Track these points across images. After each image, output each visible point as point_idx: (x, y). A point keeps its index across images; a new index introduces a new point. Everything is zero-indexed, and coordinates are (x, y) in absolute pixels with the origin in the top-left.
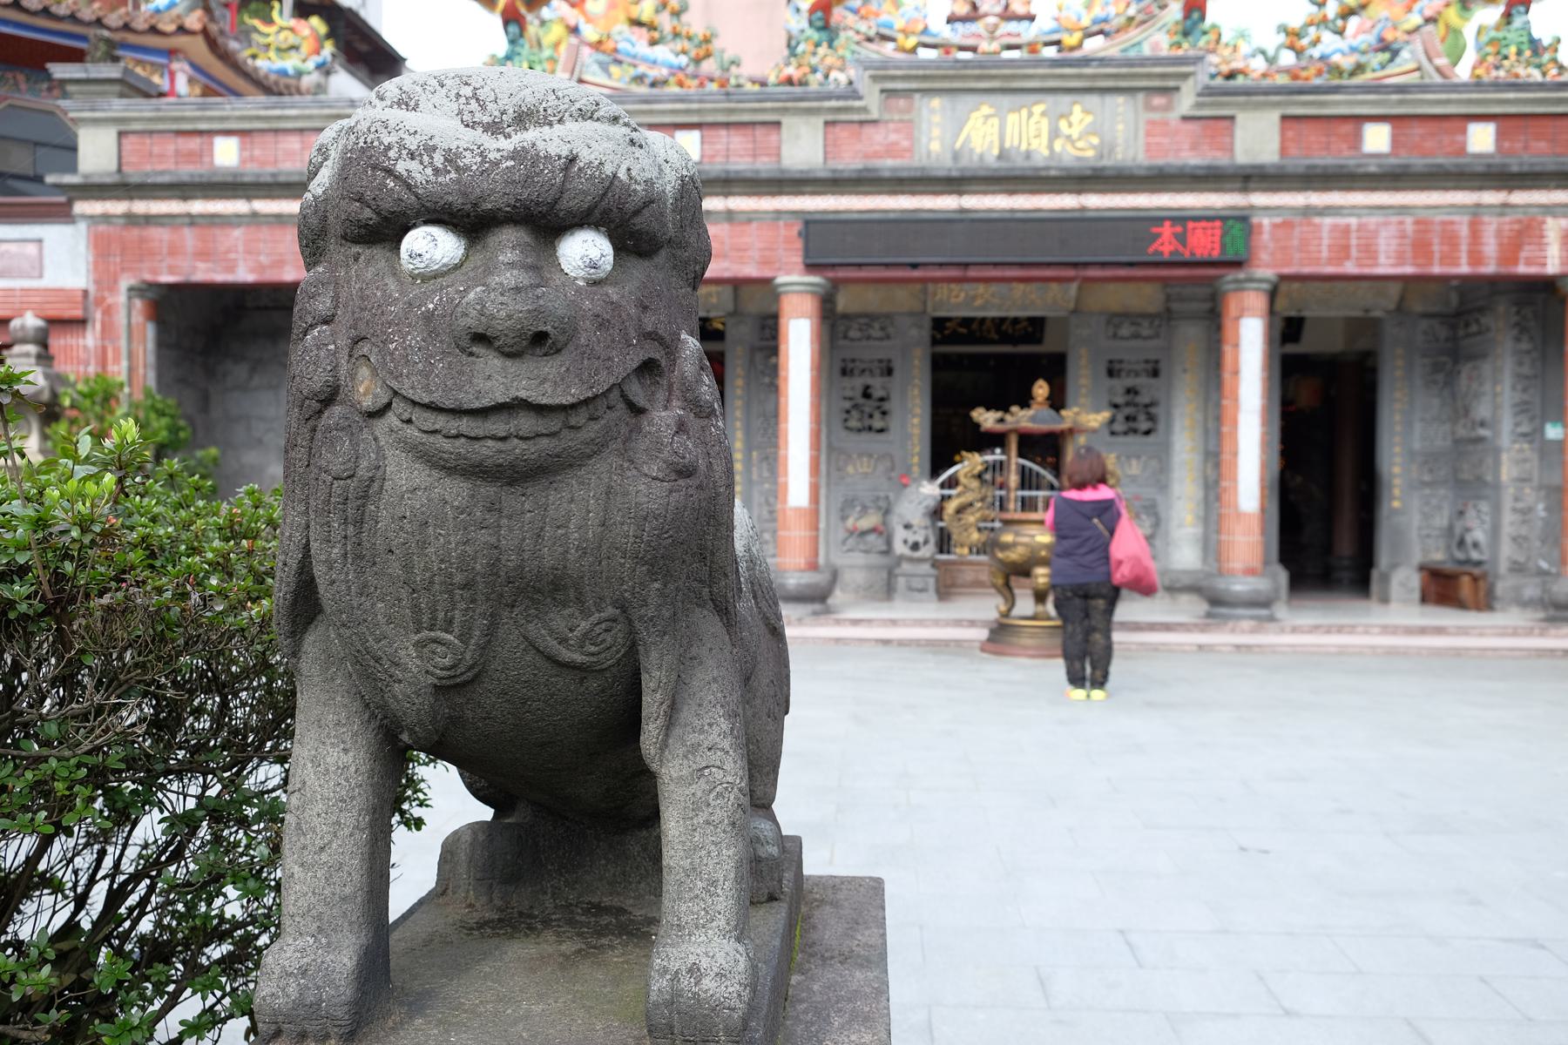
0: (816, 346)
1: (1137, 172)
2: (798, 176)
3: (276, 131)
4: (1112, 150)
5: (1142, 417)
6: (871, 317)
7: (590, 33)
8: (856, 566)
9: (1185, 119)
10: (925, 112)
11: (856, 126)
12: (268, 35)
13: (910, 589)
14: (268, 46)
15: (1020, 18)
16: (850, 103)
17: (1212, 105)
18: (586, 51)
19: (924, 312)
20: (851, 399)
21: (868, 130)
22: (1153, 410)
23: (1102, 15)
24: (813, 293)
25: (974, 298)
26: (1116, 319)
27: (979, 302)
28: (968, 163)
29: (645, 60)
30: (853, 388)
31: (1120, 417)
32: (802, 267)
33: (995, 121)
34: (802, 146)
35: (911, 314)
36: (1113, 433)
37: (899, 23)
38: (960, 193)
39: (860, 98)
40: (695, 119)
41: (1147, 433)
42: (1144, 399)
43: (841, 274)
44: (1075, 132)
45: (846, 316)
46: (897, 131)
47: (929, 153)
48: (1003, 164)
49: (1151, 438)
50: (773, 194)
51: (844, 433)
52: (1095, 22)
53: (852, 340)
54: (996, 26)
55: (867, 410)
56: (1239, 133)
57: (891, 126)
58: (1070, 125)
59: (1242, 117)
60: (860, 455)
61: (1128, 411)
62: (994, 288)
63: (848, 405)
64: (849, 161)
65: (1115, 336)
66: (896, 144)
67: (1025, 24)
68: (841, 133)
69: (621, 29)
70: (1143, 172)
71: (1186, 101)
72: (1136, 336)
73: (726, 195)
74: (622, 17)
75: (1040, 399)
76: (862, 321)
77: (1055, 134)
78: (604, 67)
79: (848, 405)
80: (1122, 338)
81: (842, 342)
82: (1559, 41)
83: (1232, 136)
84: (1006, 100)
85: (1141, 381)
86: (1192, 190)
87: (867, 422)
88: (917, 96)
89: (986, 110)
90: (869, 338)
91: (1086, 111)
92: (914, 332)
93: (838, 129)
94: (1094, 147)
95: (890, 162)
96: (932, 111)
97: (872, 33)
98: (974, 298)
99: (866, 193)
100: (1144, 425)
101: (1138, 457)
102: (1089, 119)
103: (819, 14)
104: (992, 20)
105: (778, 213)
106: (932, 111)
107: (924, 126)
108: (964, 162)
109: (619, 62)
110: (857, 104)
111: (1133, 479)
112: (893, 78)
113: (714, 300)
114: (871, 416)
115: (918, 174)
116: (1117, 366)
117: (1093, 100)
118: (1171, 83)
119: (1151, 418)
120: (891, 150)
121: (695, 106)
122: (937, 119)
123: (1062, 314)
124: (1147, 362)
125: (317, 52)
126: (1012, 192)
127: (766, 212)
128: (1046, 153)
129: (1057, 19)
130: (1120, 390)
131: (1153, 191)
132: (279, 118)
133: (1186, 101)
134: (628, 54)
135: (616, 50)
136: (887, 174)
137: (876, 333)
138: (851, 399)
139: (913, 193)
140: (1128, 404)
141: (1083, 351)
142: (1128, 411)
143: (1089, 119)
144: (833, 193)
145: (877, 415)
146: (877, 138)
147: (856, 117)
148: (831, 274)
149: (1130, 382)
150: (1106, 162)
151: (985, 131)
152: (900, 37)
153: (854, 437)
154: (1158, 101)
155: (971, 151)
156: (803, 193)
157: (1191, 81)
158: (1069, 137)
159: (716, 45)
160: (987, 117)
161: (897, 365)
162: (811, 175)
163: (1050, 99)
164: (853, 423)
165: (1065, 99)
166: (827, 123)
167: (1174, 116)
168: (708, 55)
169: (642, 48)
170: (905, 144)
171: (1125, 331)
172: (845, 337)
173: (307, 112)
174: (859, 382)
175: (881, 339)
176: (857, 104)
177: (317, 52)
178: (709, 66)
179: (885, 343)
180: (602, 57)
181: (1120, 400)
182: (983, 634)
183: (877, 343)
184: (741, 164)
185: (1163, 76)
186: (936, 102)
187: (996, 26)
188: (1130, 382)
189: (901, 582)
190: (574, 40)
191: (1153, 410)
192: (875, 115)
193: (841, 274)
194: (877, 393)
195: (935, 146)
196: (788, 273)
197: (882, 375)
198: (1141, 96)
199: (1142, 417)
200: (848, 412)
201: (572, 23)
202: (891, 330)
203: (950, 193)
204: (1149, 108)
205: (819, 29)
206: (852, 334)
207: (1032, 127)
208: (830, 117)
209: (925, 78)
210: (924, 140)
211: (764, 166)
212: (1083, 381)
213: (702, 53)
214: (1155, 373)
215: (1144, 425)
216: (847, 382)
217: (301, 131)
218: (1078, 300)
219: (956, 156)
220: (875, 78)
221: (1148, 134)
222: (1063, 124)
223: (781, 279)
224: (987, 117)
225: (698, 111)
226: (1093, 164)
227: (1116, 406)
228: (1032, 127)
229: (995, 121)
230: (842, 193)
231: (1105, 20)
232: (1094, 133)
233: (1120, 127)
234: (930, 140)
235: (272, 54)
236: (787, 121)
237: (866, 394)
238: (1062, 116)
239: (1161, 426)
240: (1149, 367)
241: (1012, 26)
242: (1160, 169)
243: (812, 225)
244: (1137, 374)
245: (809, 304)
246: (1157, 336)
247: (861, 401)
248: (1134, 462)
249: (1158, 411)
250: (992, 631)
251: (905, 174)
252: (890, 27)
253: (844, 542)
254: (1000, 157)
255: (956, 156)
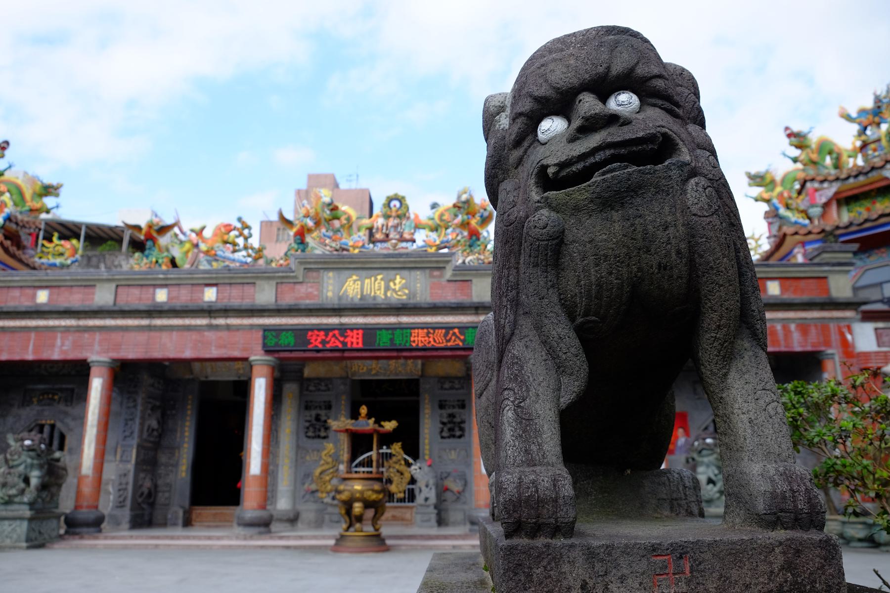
0: (269, 392)
1: (423, 306)
2: (260, 308)
3: (9, 287)
4: (415, 295)
5: (457, 429)
6: (320, 380)
7: (203, 247)
8: (308, 511)
9: (449, 281)
10: (325, 278)
11: (292, 285)
12: (47, 248)
13: (331, 521)
14: (48, 253)
15: (407, 241)
16: (288, 274)
17: (461, 275)
18: (202, 255)
19: (347, 377)
20: (309, 421)
21: (298, 287)
22: (462, 425)
23: (445, 239)
24: (268, 365)
25: (371, 370)
26: (443, 380)
27: (374, 372)
28: (345, 303)
29: (229, 259)
30: (311, 416)
31: (445, 429)
32: (263, 352)
33: (359, 283)
34: (265, 295)
35: (341, 378)
36: (442, 437)
37: (351, 243)
38: (340, 316)
39: (293, 272)
40: (214, 282)
41: (460, 437)
42: (457, 420)
43: (282, 355)
44: (397, 287)
45: (309, 380)
46: (311, 287)
47: (327, 297)
48: (362, 302)
49: (462, 440)
50: (249, 317)
51: (305, 439)
52: (442, 242)
53: (311, 391)
54: (396, 245)
55: (317, 427)
56: (474, 288)
57: (309, 285)
58: (395, 284)
59: (475, 281)
60: (313, 451)
61: (449, 426)
62: (383, 362)
63: (307, 424)
64: (288, 300)
65: (442, 388)
66: (311, 293)
67: (410, 243)
68: (285, 288)
69: (219, 245)
70: (426, 306)
71: (448, 274)
72: (452, 388)
73: (227, 317)
74: (220, 240)
75: (363, 415)
76: (316, 381)
77: (387, 288)
78: (209, 262)
79: (307, 424)
80: (446, 389)
81: (305, 393)
82: (61, 186)
83: (471, 290)
84: (364, 273)
85: (456, 411)
86: (452, 314)
87: (317, 433)
88: (322, 271)
89: (355, 277)
90: (319, 390)
91: (402, 278)
92: (342, 387)
93: (284, 286)
94: (406, 294)
95: (308, 302)
96: (329, 278)
97: (338, 247)
98: (371, 370)
99: (295, 316)
100: (458, 433)
101: (455, 449)
102: (404, 281)
103: (298, 237)
104: (394, 241)
105: (252, 326)
106: (329, 278)
107: (325, 285)
108: (344, 302)
109: (217, 260)
110: (292, 274)
111: (453, 461)
112: (310, 263)
113: (241, 372)
114: (320, 430)
115: (318, 307)
116: (444, 403)
117: (406, 273)
118: (441, 265)
119: (462, 429)
120: (309, 296)
121: (214, 276)
122: (331, 281)
123: (416, 377)
124: (458, 401)
125: (73, 256)
126: (365, 316)
127: (246, 325)
128: (383, 297)
129: (424, 241)
130: (445, 415)
131: (433, 315)
132: (10, 281)
133: (448, 274)
134: (221, 257)
135: (216, 255)
136: (303, 307)
137: (323, 388)
138: (309, 421)
139: (318, 316)
140: (450, 422)
141: (427, 396)
142: (449, 426)
143: (404, 281)
144: (279, 316)
145: (323, 430)
146: (302, 290)
147: (291, 281)
148: (277, 355)
149: (450, 411)
150: (412, 301)
151: (353, 287)
152: (351, 249)
153: (310, 441)
154: (436, 273)
155: (347, 296)
156: (264, 316)
157: (450, 264)
158: (394, 290)
159: (265, 252)
160: (355, 281)
161: (333, 404)
162: (266, 308)
163: (385, 272)
164: (310, 434)
165: (393, 272)
166: (277, 283)
167: (443, 281)
168: (261, 257)
169: (228, 254)
170: (316, 293)
171: (447, 386)
172: (307, 390)
173: (24, 278)
174: (314, 413)
175: (325, 391)
176: (292, 274)
177: (73, 256)
178: (261, 262)
179: (327, 393)
180: (208, 258)
181: (445, 420)
182: (332, 542)
183: (324, 393)
184: (236, 302)
185: (437, 262)
186: (331, 274)
187: (396, 245)
188: (450, 411)
189: (327, 517)
190: (196, 250)
191: (462, 425)
192: (301, 280)
193: (282, 355)
194: (323, 418)
195: (330, 294)
196: (255, 355)
197: (326, 409)
198: (427, 271)
199: (457, 429)
200: (308, 428)
201: (195, 242)
202: (330, 386)
203: (336, 316)
204: (432, 276)
205: (298, 244)
206: (312, 388)
207: (377, 285)
208: (279, 281)
209: (325, 263)
210: (325, 291)
211: (246, 303)
212: (427, 411)
213: (257, 256)
214: (463, 406)
215: (458, 433)
216: (307, 413)
217: (21, 287)
218: (423, 370)
219: (340, 298)
220: (301, 263)
221: (431, 288)
222: (392, 284)
223: (252, 358)
224: (355, 281)
225: (216, 278)
226: (405, 302)
227: (444, 424)
228: (377, 285)
229: (359, 283)
230: (283, 316)
231: (447, 242)
232: (406, 288)
233: (418, 285)
234: (328, 291)
235: (50, 257)
236: (258, 282)
237: (318, 418)
238: (390, 280)
239: (466, 434)
240: (460, 403)
241: (404, 244)
242: (435, 304)
243: (266, 330)
244: (454, 407)
245: (265, 370)
246: (462, 388)
247: (314, 422)
248: (453, 452)
249: (465, 426)
250: (337, 540)
251: (312, 307)
252: (346, 245)
253: (304, 497)
254: (361, 299)
255: (340, 298)
